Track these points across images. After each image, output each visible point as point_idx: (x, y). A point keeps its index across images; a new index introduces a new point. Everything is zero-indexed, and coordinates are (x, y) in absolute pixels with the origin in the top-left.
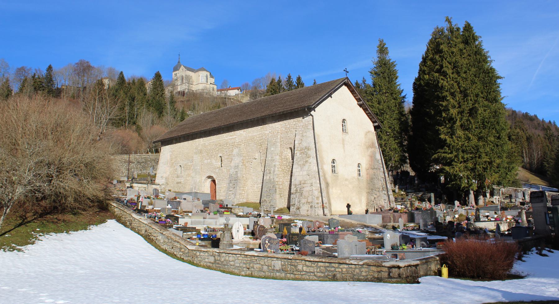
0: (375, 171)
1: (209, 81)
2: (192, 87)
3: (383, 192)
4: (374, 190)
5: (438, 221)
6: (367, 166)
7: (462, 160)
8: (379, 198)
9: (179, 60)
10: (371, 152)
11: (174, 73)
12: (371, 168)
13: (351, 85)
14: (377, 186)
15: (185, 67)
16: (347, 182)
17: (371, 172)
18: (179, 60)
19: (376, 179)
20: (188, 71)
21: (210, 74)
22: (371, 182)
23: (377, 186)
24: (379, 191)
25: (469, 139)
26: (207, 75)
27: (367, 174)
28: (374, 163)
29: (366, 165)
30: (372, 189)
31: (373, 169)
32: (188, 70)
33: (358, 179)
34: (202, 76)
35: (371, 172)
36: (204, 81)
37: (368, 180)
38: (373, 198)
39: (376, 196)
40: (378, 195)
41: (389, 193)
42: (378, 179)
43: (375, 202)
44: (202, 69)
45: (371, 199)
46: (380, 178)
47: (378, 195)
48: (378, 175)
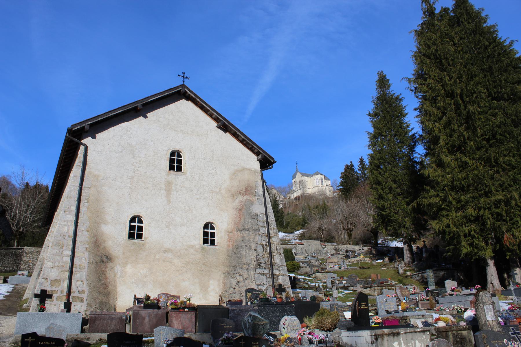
0: (245, 233)
1: (324, 183)
2: (306, 191)
3: (259, 271)
4: (238, 268)
5: (471, 321)
6: (230, 226)
7: (459, 205)
8: (246, 282)
9: (297, 168)
10: (240, 202)
11: (293, 181)
12: (238, 230)
13: (194, 96)
14: (244, 260)
15: (301, 173)
16: (170, 255)
17: (237, 235)
18: (297, 168)
19: (245, 248)
20: (304, 177)
21: (325, 177)
22: (235, 253)
23: (244, 260)
24: (247, 269)
25: (464, 166)
26: (321, 178)
27: (229, 240)
28: (244, 220)
29: (228, 225)
30: (235, 267)
31: (241, 231)
32: (303, 176)
33: (203, 249)
34: (317, 180)
35: (237, 235)
36: (320, 184)
37: (228, 251)
38: (234, 282)
39: (240, 279)
40: (245, 275)
41: (276, 272)
42: (250, 248)
43: (237, 289)
44: (317, 173)
45: (231, 284)
46: (253, 246)
47: (245, 275)
48: (249, 241)
